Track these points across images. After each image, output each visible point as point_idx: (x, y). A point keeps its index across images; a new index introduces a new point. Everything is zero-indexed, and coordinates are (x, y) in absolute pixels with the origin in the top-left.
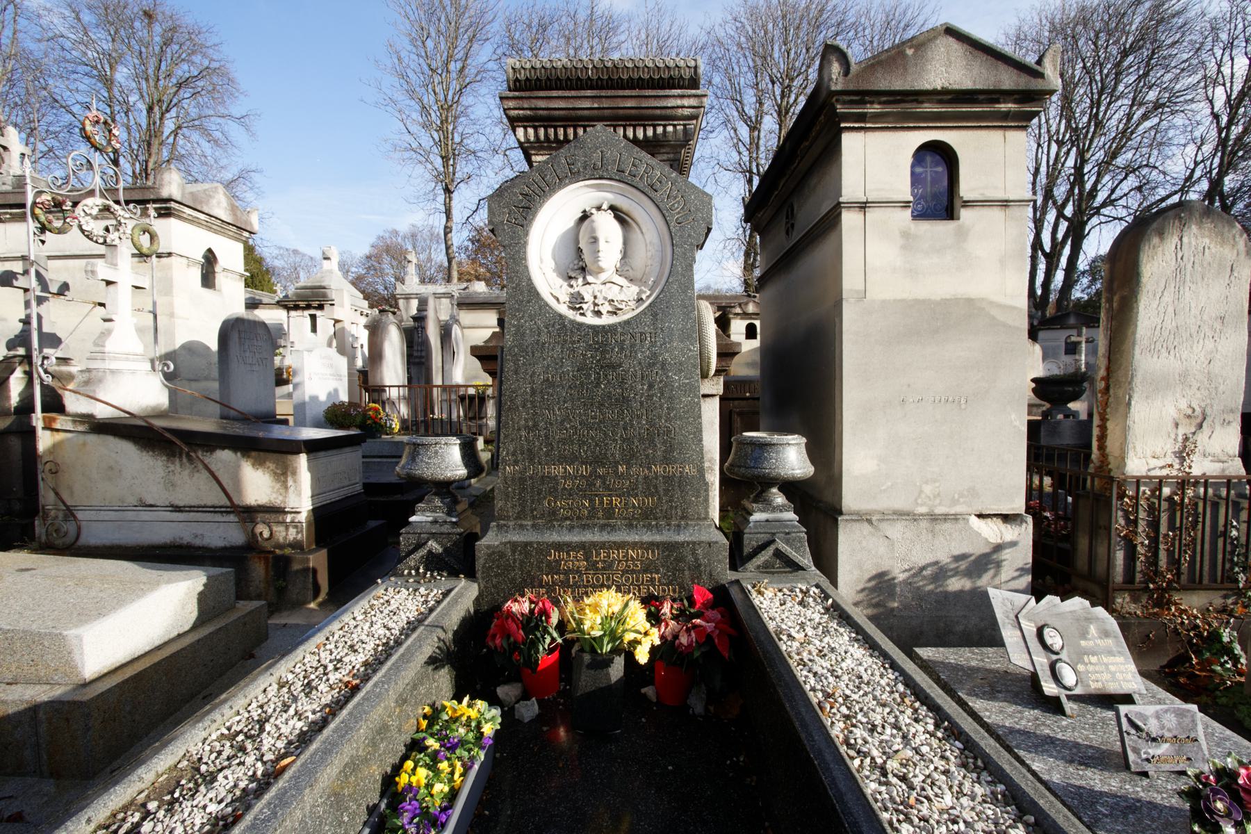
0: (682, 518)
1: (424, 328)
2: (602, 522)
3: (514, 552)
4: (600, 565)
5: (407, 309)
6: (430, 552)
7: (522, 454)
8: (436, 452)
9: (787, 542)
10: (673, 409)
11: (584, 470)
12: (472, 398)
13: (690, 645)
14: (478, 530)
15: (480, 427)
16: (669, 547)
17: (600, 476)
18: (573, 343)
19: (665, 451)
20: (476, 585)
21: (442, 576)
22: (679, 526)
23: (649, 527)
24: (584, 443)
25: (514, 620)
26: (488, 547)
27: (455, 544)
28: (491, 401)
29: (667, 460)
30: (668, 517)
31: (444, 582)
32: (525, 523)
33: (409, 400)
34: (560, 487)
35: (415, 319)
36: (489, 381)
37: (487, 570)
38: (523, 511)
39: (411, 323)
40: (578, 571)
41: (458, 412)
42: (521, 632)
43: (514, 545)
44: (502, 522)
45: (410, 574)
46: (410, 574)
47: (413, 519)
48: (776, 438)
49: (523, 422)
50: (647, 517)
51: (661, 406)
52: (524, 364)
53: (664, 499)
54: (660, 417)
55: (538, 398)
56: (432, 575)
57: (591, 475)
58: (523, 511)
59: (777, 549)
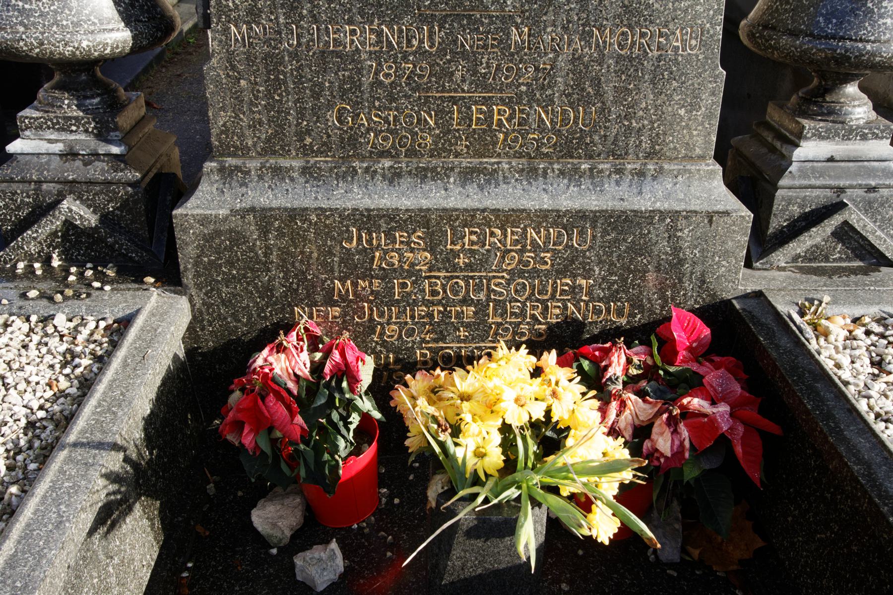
0: (649, 155)
2: (465, 162)
3: (264, 232)
4: (462, 261)
6: (68, 224)
11: (425, 39)
13: (678, 453)
16: (620, 222)
17: (464, 55)
20: (183, 303)
23: (573, 175)
25: (279, 397)
26: (204, 220)
27: (125, 205)
30: (617, 153)
31: (114, 300)
32: (285, 163)
40: (412, 272)
42: (299, 419)
43: (264, 218)
44: (230, 161)
45: (30, 270)
46: (30, 270)
47: (14, 147)
50: (572, 151)
53: (615, 111)
56: (81, 275)
57: (442, 52)
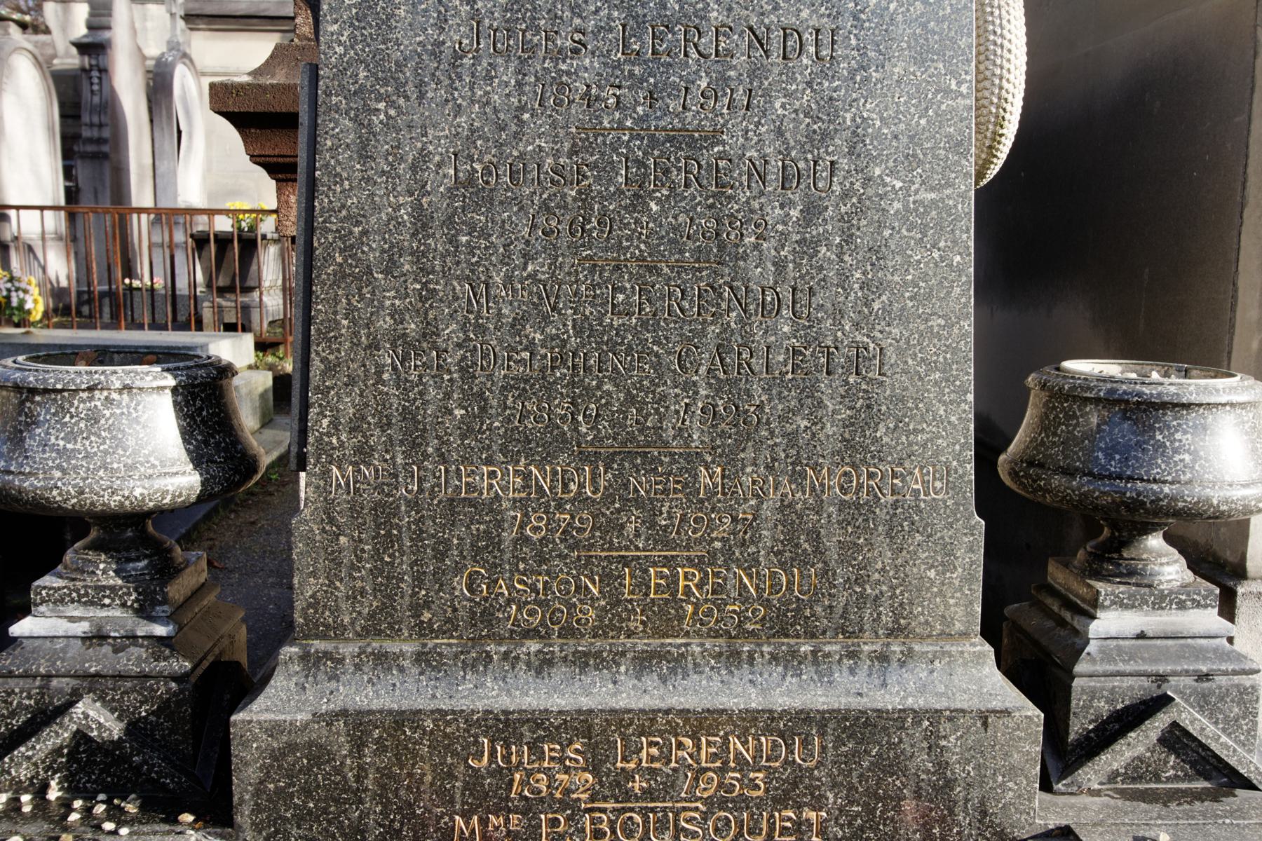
0: (895, 631)
1: (104, 71)
2: (641, 644)
4: (637, 785)
5: (64, 28)
6: (81, 737)
7: (385, 426)
8: (93, 418)
9: (1203, 702)
10: (881, 287)
11: (583, 482)
12: (223, 241)
14: (236, 636)
15: (246, 309)
16: (859, 727)
17: (638, 502)
18: (560, 55)
19: (848, 424)
21: (116, 814)
22: (883, 658)
23: (790, 661)
24: (588, 392)
26: (274, 729)
27: (164, 708)
28: (273, 250)
29: (854, 449)
32: (392, 647)
33: (73, 239)
34: (508, 536)
35: (83, 48)
36: (262, 191)
37: (269, 802)
38: (387, 606)
39: (71, 60)
40: (567, 804)
41: (192, 275)
43: (359, 724)
44: (318, 645)
47: (21, 628)
48: (1161, 382)
49: (385, 323)
50: (786, 627)
51: (844, 277)
52: (389, 124)
54: (838, 313)
55: (438, 243)
57: (608, 499)
58: (387, 606)
59: (1175, 725)
